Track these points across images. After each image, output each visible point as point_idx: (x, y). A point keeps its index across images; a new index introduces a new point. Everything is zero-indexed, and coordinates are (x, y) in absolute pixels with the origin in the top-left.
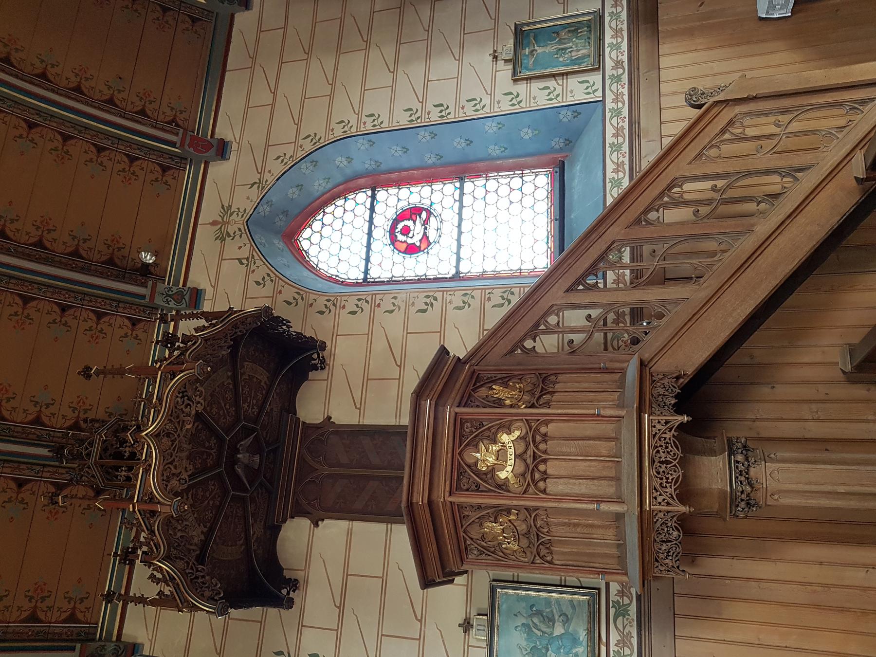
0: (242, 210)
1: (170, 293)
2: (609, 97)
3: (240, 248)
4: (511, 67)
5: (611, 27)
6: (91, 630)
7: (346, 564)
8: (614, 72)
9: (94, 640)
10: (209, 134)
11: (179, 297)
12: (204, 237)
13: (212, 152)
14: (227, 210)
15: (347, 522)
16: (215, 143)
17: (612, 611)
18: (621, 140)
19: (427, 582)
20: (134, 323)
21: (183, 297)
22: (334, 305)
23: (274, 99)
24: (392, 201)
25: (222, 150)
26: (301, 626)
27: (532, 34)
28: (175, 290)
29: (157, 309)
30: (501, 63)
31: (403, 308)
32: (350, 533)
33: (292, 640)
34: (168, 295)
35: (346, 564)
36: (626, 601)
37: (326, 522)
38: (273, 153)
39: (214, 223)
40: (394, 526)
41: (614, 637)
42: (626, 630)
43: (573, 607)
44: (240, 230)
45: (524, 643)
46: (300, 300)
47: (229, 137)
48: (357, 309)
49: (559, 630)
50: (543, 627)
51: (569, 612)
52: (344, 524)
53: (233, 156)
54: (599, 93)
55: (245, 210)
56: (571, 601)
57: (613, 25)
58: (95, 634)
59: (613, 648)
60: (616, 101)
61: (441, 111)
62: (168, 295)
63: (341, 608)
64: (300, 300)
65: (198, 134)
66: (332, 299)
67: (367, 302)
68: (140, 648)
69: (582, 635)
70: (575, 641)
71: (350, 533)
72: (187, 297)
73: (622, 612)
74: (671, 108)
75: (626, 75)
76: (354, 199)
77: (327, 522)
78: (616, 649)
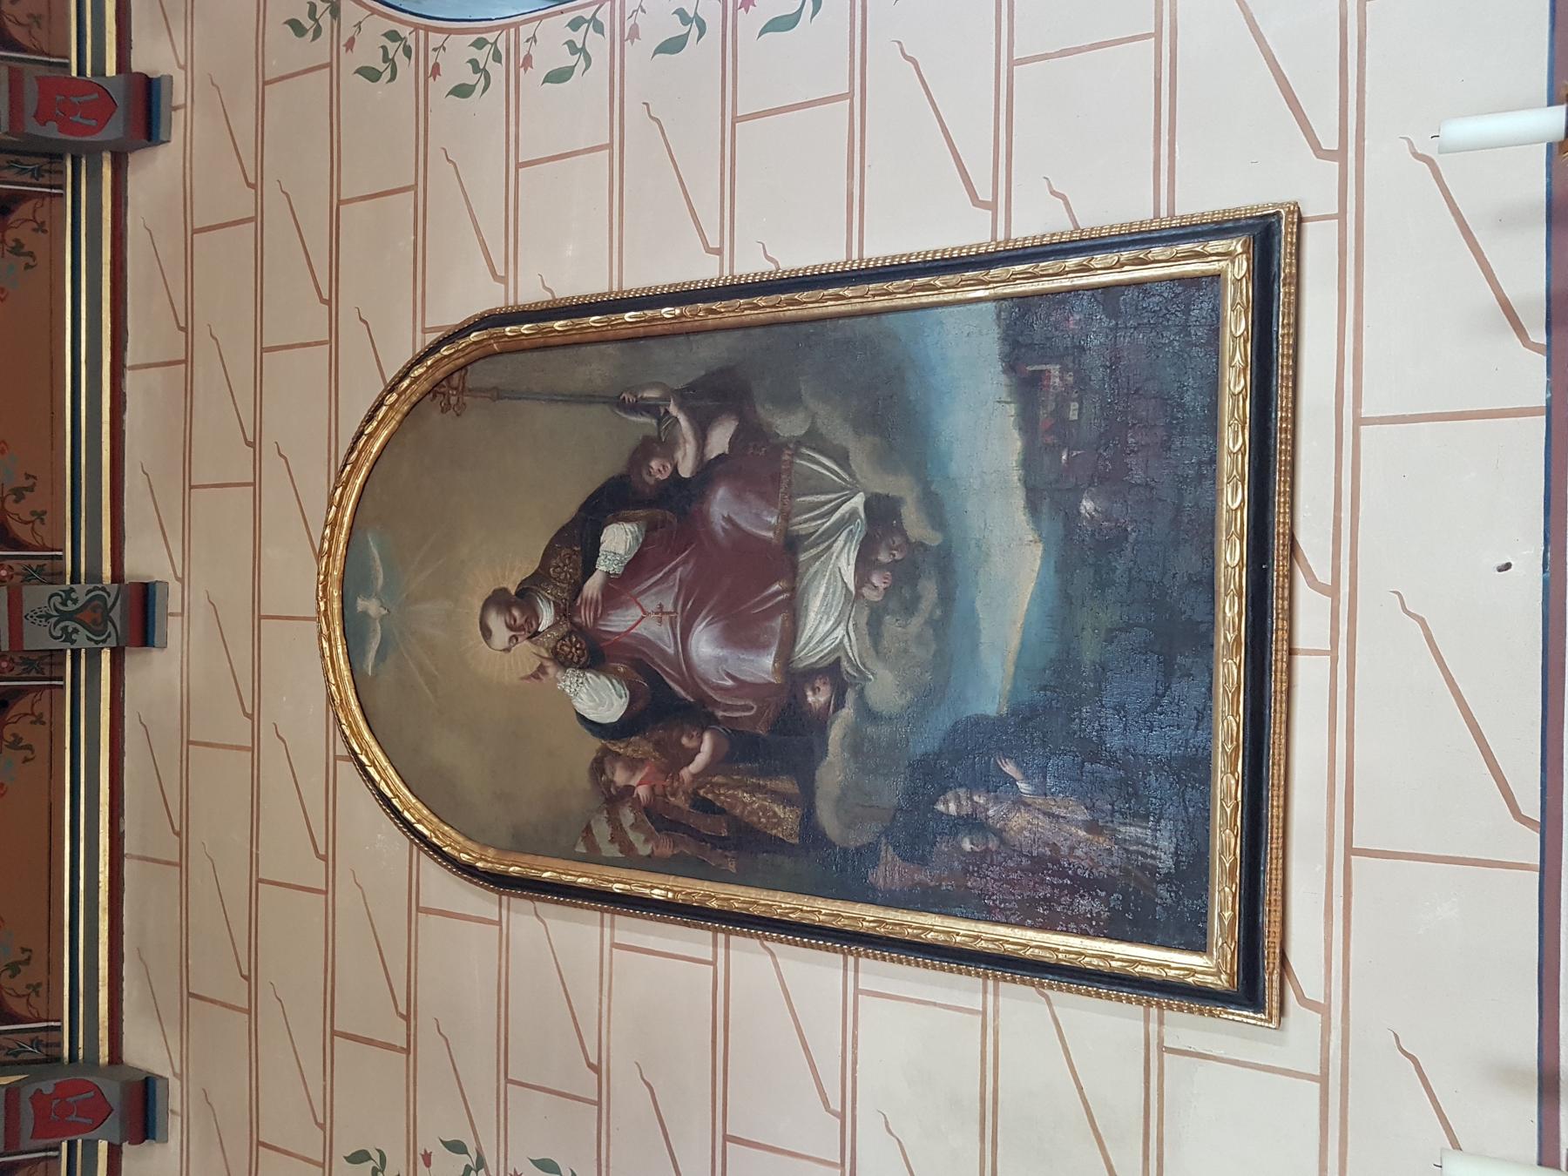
1: (71, 607)
11: (94, 616)
13: (114, 130)
16: (112, 1091)
19: (1267, 239)
21: (107, 611)
27: (1163, 847)
28: (82, 592)
31: (714, 27)
34: (64, 616)
46: (400, 59)
48: (571, 60)
53: (174, 1126)
62: (64, 616)
64: (400, 59)
65: (81, 70)
66: (490, 37)
67: (599, 28)
68: (164, 92)
72: (116, 614)
77: (817, 773)
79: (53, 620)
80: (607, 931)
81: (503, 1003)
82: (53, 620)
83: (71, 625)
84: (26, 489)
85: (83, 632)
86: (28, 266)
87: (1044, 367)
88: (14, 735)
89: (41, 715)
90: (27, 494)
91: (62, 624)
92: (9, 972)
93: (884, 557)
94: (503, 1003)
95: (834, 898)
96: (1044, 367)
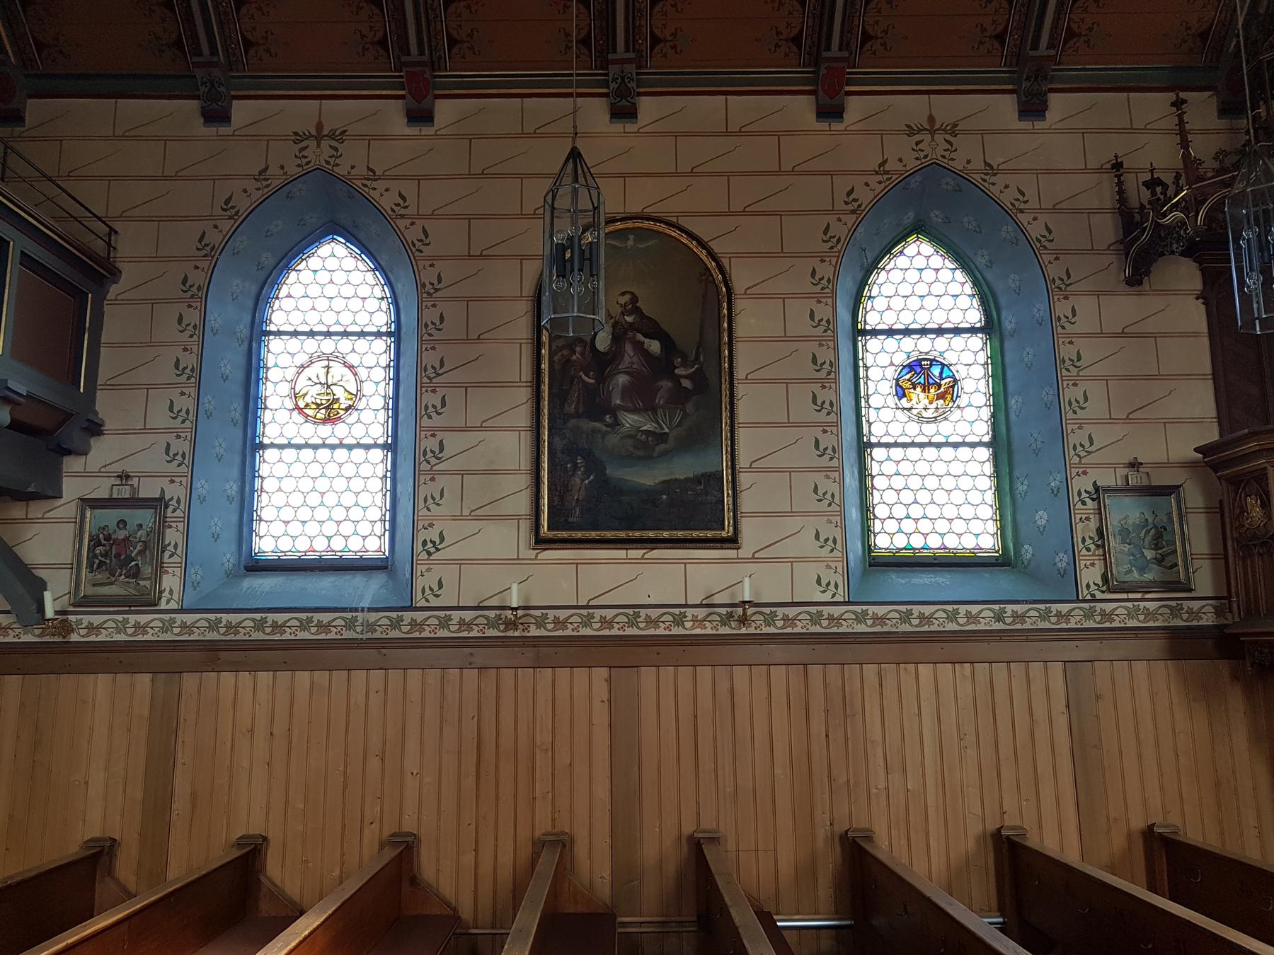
0: (953, 155)
2: (420, 616)
3: (900, 160)
4: (1119, 483)
5: (981, 611)
6: (443, 65)
7: (1165, 335)
8: (690, 618)
9: (434, 70)
10: (1053, 86)
12: (913, 107)
14: (339, 136)
15: (1206, 330)
17: (1173, 603)
18: (1054, 620)
20: (797, 40)
22: (192, 297)
23: (683, 174)
24: (370, 360)
25: (830, 112)
26: (1098, 294)
29: (816, 65)
30: (1122, 472)
31: (818, 375)
32: (1196, 335)
33: (1083, 286)
34: (623, 78)
35: (1165, 335)
36: (268, 630)
37: (1203, 307)
38: (409, 188)
39: (931, 119)
40: (1209, 384)
41: (1152, 606)
42: (707, 624)
43: (1171, 567)
44: (309, 163)
45: (1130, 521)
47: (1053, 115)
49: (1149, 554)
50: (1148, 539)
51: (1167, 563)
52: (1204, 327)
54: (422, 603)
55: (952, 159)
56: (1176, 565)
57: (1032, 613)
58: (440, 70)
59: (1142, 604)
60: (1015, 615)
61: (1077, 401)
62: (623, 78)
63: (1123, 334)
69: (1148, 576)
70: (1142, 570)
71: (1196, 335)
72: (214, 106)
73: (1175, 612)
74: (1113, 674)
75: (956, 628)
76: (380, 309)
78: (916, 614)
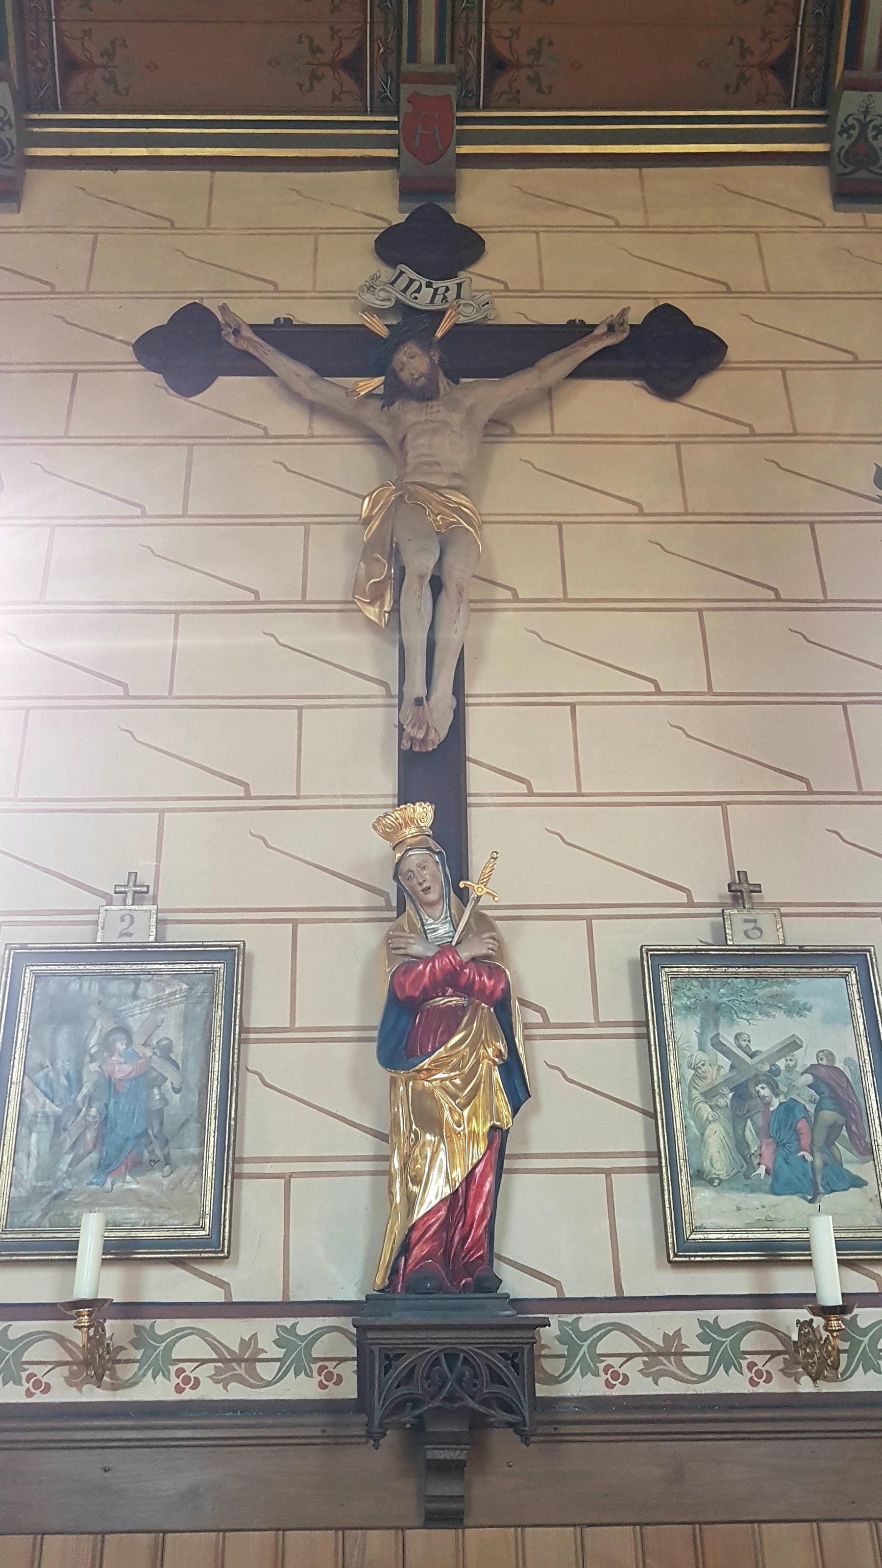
1: (871, 134)
34: (864, 126)
62: (864, 126)
72: (862, 174)
79: (862, 117)
80: (631, 1030)
81: (49, 655)
82: (862, 117)
83: (855, 133)
84: (311, 43)
85: (848, 144)
86: (727, 87)
87: (546, 1316)
88: (528, 53)
89: (83, 31)
90: (314, 44)
91: (857, 125)
92: (748, 56)
93: (86, 985)
94: (49, 655)
95: (31, 1403)
96: (546, 1316)
